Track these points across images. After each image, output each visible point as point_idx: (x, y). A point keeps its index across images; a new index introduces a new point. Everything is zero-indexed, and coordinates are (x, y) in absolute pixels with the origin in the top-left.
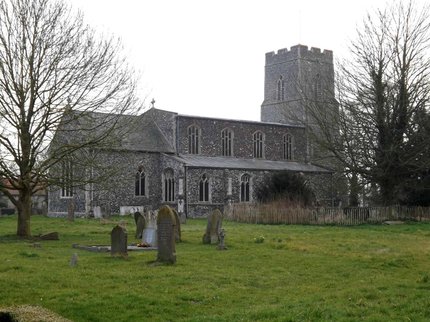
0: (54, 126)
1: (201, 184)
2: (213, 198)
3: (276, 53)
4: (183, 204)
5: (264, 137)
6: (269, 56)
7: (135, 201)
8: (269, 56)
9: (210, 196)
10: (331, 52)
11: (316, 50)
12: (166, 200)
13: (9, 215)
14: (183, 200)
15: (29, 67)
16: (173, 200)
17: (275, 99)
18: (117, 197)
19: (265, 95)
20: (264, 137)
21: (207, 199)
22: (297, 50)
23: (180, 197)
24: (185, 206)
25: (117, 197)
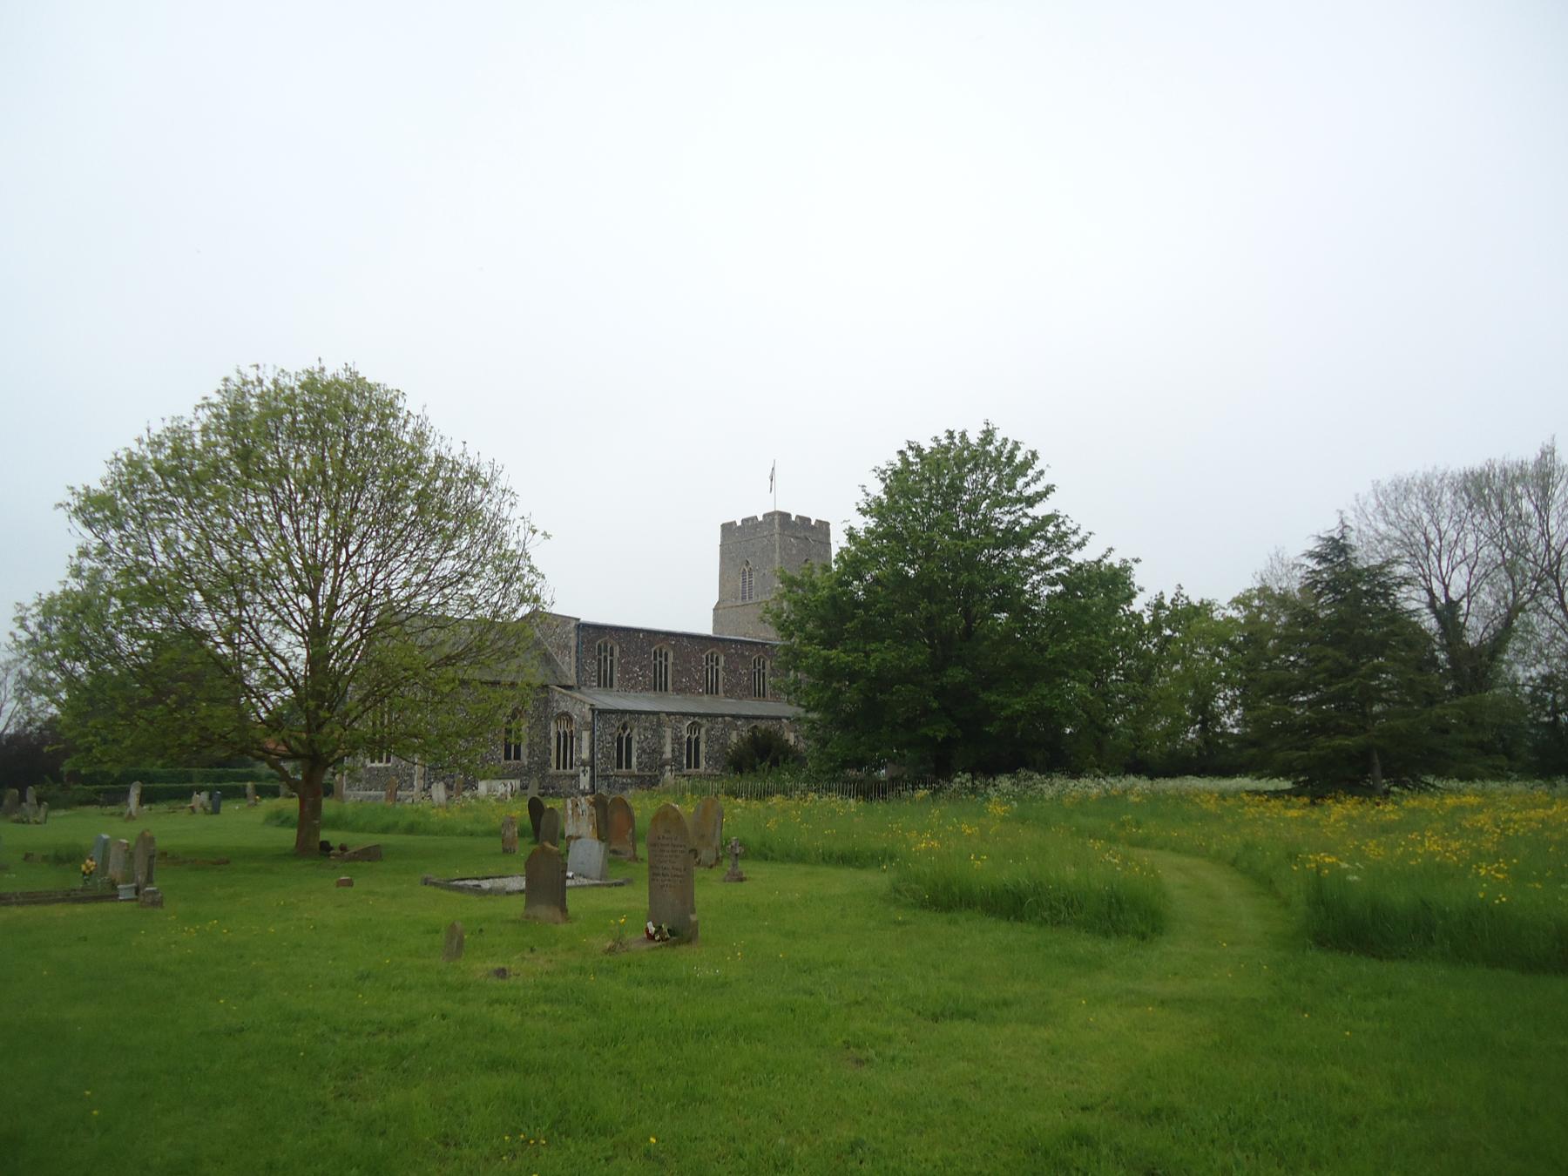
2: (640, 763)
3: (739, 523)
4: (588, 775)
5: (722, 659)
6: (727, 529)
8: (727, 529)
9: (634, 760)
14: (588, 768)
19: (721, 592)
20: (722, 659)
21: (629, 766)
24: (592, 778)
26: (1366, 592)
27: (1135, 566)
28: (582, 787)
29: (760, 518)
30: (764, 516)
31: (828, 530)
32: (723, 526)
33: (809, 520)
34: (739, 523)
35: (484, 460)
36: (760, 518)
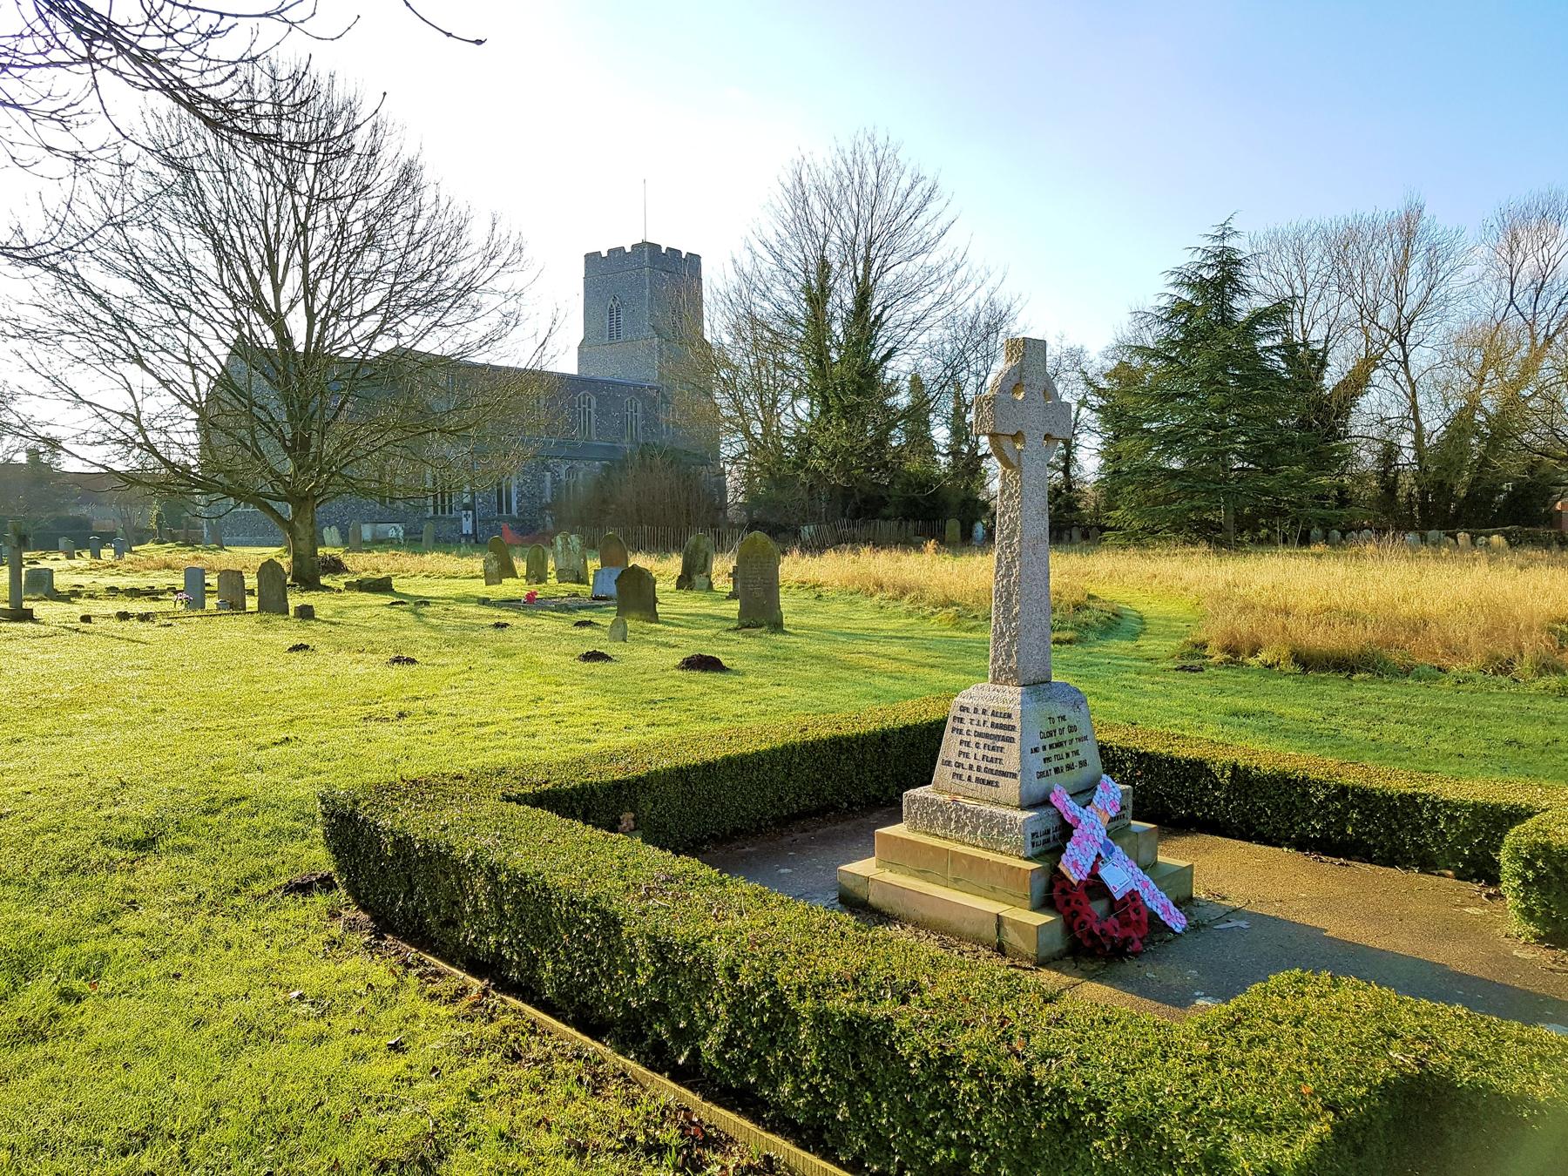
0: (301, 307)
1: (500, 491)
2: (520, 508)
3: (604, 254)
4: (470, 519)
5: (594, 401)
6: (592, 259)
7: (380, 514)
8: (592, 259)
9: (514, 504)
10: (698, 257)
11: (674, 253)
12: (436, 512)
13: (652, 1068)
14: (470, 512)
15: (96, 470)
16: (451, 512)
17: (603, 336)
18: (346, 508)
19: (585, 329)
20: (594, 401)
21: (509, 510)
22: (643, 252)
23: (467, 507)
24: (474, 522)
25: (346, 508)
26: (1375, 846)
27: (1231, 243)
28: (465, 532)
29: (628, 250)
30: (609, 251)
31: (699, 263)
32: (587, 256)
33: (680, 252)
34: (604, 254)
35: (1206, 243)
36: (628, 250)
